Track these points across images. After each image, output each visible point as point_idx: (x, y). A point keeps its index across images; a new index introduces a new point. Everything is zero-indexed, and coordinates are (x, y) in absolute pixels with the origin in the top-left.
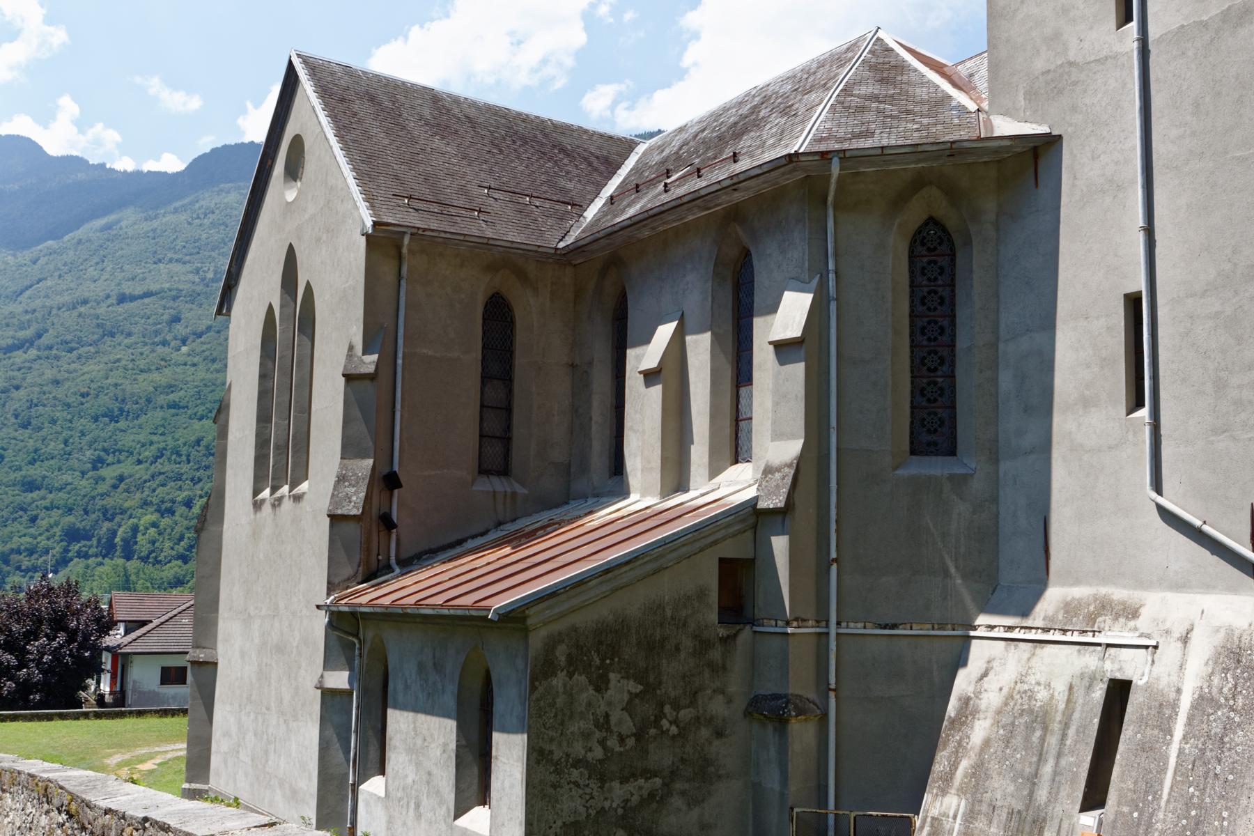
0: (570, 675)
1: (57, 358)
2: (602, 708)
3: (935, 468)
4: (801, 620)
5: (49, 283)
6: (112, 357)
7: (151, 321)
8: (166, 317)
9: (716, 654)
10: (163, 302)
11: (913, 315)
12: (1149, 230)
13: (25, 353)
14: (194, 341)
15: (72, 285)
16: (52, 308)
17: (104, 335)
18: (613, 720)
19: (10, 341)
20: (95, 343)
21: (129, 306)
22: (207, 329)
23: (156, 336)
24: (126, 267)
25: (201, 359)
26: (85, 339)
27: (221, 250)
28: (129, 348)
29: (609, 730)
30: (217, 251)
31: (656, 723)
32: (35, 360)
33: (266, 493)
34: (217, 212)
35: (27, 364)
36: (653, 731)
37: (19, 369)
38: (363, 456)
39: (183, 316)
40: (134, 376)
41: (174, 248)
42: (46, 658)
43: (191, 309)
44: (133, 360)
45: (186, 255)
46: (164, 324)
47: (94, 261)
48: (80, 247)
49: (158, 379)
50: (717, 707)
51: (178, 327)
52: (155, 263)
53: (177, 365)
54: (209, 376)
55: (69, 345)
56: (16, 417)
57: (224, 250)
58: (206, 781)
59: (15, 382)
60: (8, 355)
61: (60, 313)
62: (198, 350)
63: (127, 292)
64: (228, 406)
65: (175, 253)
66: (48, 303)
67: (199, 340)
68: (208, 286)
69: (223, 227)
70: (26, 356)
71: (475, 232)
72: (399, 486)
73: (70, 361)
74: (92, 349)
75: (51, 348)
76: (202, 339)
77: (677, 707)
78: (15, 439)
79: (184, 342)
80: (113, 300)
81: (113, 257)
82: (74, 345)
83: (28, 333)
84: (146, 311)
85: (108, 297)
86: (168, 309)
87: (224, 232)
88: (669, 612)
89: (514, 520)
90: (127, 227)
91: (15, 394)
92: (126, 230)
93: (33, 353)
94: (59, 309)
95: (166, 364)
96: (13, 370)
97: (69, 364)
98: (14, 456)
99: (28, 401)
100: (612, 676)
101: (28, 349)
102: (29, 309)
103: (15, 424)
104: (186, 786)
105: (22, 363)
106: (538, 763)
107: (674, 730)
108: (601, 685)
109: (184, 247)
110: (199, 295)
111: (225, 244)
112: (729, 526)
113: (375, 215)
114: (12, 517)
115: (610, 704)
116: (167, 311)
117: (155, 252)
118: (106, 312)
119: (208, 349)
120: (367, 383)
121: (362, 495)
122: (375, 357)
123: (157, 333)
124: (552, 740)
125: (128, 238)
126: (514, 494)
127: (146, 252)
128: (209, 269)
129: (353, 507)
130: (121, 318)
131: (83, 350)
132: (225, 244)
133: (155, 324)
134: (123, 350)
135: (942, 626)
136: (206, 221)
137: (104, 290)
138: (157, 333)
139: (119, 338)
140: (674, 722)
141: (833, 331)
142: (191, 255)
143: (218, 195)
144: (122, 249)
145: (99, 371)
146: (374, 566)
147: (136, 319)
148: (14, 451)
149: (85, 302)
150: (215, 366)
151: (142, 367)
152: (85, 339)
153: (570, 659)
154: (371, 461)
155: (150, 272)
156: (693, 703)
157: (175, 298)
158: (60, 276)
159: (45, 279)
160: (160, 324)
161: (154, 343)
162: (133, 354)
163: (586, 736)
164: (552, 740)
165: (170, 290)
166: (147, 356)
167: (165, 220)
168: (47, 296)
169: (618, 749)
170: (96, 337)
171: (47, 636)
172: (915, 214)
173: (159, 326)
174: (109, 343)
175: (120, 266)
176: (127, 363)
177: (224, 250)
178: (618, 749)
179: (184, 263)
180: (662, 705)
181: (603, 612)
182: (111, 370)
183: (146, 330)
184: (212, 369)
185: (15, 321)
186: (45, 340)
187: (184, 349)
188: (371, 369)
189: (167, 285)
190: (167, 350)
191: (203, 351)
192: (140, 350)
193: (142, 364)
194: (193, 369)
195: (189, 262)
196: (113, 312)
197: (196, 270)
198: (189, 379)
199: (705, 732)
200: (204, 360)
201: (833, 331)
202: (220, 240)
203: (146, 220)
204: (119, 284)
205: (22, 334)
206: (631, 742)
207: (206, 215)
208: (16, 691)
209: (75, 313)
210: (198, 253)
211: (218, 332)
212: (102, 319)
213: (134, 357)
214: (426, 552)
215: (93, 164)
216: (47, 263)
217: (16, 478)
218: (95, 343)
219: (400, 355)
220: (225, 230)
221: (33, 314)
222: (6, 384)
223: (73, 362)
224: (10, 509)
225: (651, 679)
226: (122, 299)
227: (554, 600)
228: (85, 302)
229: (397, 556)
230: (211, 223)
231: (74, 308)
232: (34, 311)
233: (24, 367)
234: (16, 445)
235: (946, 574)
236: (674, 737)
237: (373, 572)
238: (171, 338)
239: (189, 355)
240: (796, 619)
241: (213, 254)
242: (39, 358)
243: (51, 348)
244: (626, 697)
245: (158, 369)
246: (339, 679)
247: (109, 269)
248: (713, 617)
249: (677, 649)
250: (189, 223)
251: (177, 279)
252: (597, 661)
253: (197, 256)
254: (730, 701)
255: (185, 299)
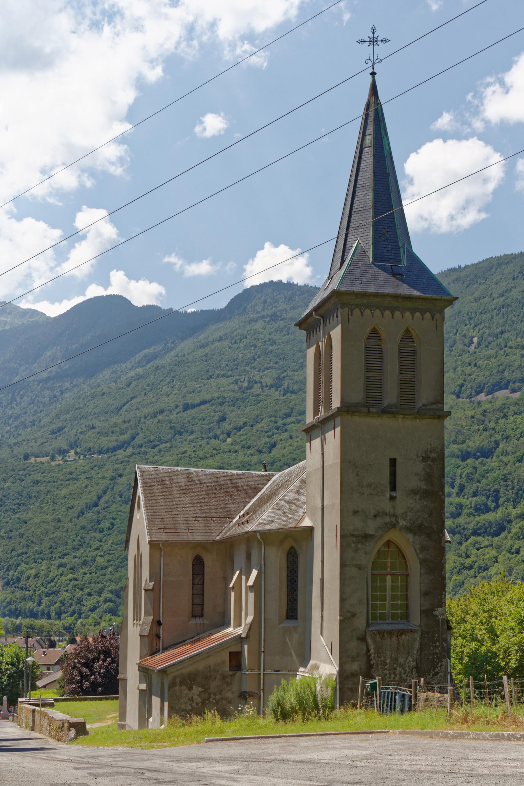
0: (181, 686)
1: (145, 453)
2: (191, 695)
3: (290, 623)
4: (252, 670)
5: (139, 399)
6: (182, 450)
7: (206, 422)
8: (216, 418)
9: (228, 680)
10: (214, 407)
11: (288, 576)
12: (322, 561)
13: (125, 451)
14: (235, 434)
15: (154, 400)
16: (140, 418)
17: (176, 434)
18: (194, 699)
19: (115, 444)
20: (169, 440)
21: (191, 412)
22: (244, 424)
23: (210, 432)
24: (189, 383)
25: (240, 447)
26: (163, 438)
27: (253, 365)
28: (192, 442)
29: (193, 701)
30: (249, 366)
31: (208, 699)
32: (131, 456)
33: (135, 621)
34: (249, 337)
35: (126, 459)
36: (207, 702)
37: (121, 463)
38: (150, 615)
39: (227, 416)
40: (195, 463)
41: (220, 367)
42: (102, 671)
43: (233, 411)
44: (195, 451)
45: (229, 371)
46: (215, 423)
47: (167, 381)
48: (158, 372)
49: (212, 463)
50: (229, 695)
51: (224, 424)
52: (208, 379)
53: (224, 452)
54: (246, 459)
55: (153, 443)
56: (121, 496)
57: (255, 364)
58: (125, 721)
59: (120, 472)
60: (114, 453)
61: (146, 421)
62: (238, 440)
63: (189, 402)
64: (128, 586)
65: (221, 370)
66: (139, 414)
67: (238, 433)
68: (244, 393)
69: (253, 348)
70: (125, 453)
71: (185, 538)
72: (161, 624)
73: (153, 454)
74: (168, 445)
75: (140, 446)
76: (241, 432)
77: (215, 695)
78: (120, 511)
79: (229, 435)
80: (180, 409)
81: (179, 377)
82: (156, 443)
83: (126, 437)
84: (202, 414)
85: (177, 406)
86: (217, 412)
87: (254, 352)
88: (212, 668)
89: (204, 632)
90: (188, 354)
91: (119, 480)
92: (187, 357)
93: (130, 450)
94: (145, 418)
95: (217, 452)
96: (117, 464)
97: (153, 457)
98: (121, 523)
99: (127, 485)
100: (194, 686)
101: (126, 448)
102: (126, 420)
103: (120, 501)
104: (119, 723)
105: (123, 458)
106: (171, 710)
107: (214, 701)
108: (190, 688)
109: (227, 365)
110: (238, 400)
111: (255, 360)
112: (232, 642)
113: (151, 538)
114: (121, 565)
115: (193, 694)
116: (217, 414)
117: (207, 371)
118: (176, 418)
119: (245, 440)
120: (151, 592)
121: (149, 628)
122: (153, 583)
123: (210, 430)
124: (175, 704)
125: (189, 362)
126: (204, 624)
127: (201, 371)
128: (244, 380)
129: (146, 633)
130: (186, 421)
131: (162, 446)
132: (255, 360)
133: (209, 424)
134: (189, 444)
135: (291, 671)
136: (241, 344)
137: (174, 402)
138: (210, 430)
139: (185, 435)
140: (214, 699)
141: (263, 583)
142: (232, 370)
143: (249, 324)
144: (186, 371)
145: (173, 461)
146: (154, 650)
147: (196, 421)
148: (120, 520)
149: (162, 412)
150: (250, 451)
151: (201, 456)
152: (163, 438)
153: (180, 682)
154: (152, 617)
155: (204, 385)
156: (220, 693)
157: (221, 404)
158: (145, 394)
159: (136, 397)
160: (212, 423)
161: (208, 438)
162: (194, 447)
163: (186, 703)
164: (175, 704)
165: (218, 398)
166: (204, 447)
167: (213, 347)
168: (137, 409)
169: (196, 706)
170: (170, 436)
171: (102, 660)
172: (287, 546)
173: (211, 425)
174: (178, 440)
175: (184, 383)
176: (191, 453)
177: (255, 364)
178: (196, 706)
179: (227, 377)
180: (210, 694)
181: (191, 669)
182: (181, 460)
183: (203, 428)
184: (248, 454)
185: (117, 429)
186: (138, 441)
187: (229, 440)
188: (151, 587)
189: (216, 395)
190: (217, 442)
191: (242, 441)
192: (199, 443)
193: (200, 453)
194: (235, 454)
195: (231, 376)
196: (180, 417)
197: (236, 381)
198: (233, 462)
199: (224, 702)
200: (242, 447)
201: (263, 583)
202: (251, 358)
203: (201, 348)
204: (185, 396)
205: (123, 438)
206: (200, 705)
207: (241, 340)
208: (91, 687)
209: (156, 420)
210: (237, 369)
211: (252, 426)
212: (174, 423)
213: (195, 449)
214: (172, 645)
215: (164, 310)
216: (136, 386)
217: (122, 538)
218: (169, 440)
219: (162, 581)
220: (254, 350)
221: (129, 423)
222: (113, 474)
223: (156, 455)
224: (119, 560)
225: (207, 687)
226: (187, 407)
227: (174, 666)
228: (162, 412)
229: (162, 646)
230: (245, 346)
231: (155, 416)
232: (130, 420)
233: (124, 461)
234: (121, 516)
235: (292, 656)
236: (214, 703)
237: (153, 653)
238: (220, 432)
239: (232, 444)
240: (250, 669)
241: (247, 368)
242: (134, 454)
243: (140, 446)
244: (198, 692)
245: (211, 456)
246: (143, 686)
247: (177, 386)
248: (228, 669)
249: (215, 678)
250: (230, 348)
251: (223, 389)
252: (189, 682)
253: (236, 371)
254: (233, 693)
255: (229, 404)
